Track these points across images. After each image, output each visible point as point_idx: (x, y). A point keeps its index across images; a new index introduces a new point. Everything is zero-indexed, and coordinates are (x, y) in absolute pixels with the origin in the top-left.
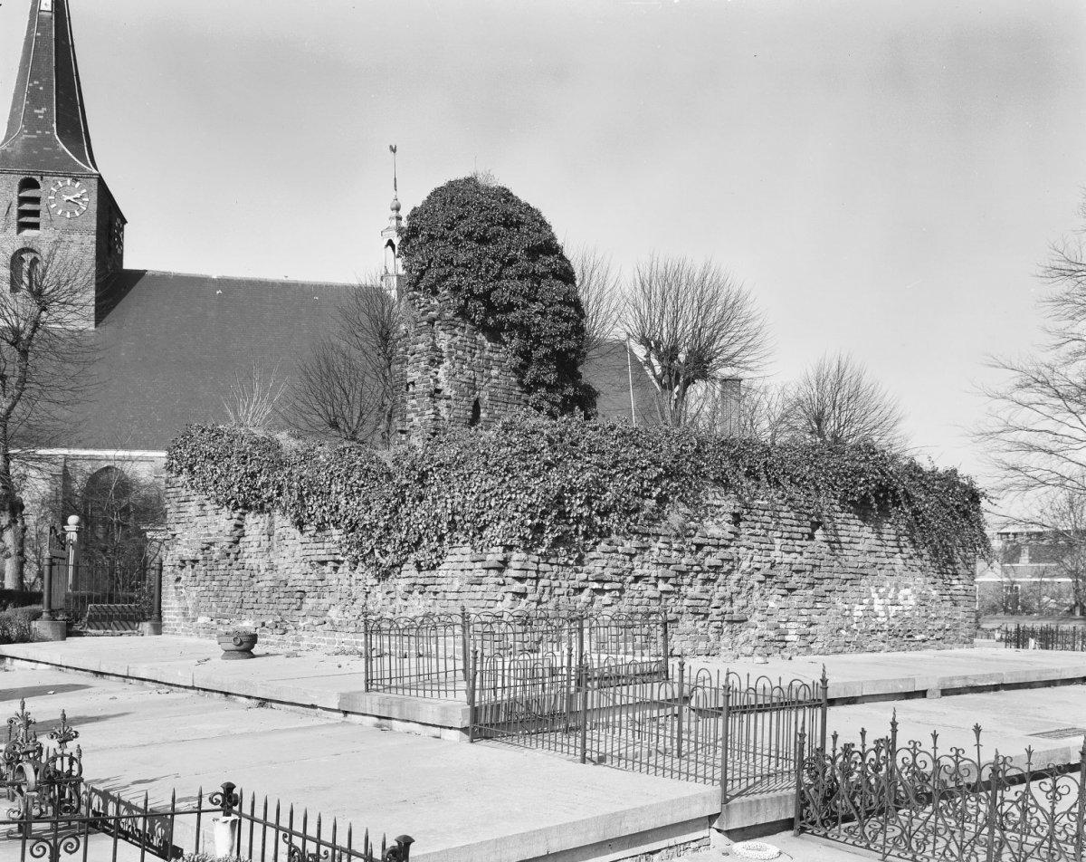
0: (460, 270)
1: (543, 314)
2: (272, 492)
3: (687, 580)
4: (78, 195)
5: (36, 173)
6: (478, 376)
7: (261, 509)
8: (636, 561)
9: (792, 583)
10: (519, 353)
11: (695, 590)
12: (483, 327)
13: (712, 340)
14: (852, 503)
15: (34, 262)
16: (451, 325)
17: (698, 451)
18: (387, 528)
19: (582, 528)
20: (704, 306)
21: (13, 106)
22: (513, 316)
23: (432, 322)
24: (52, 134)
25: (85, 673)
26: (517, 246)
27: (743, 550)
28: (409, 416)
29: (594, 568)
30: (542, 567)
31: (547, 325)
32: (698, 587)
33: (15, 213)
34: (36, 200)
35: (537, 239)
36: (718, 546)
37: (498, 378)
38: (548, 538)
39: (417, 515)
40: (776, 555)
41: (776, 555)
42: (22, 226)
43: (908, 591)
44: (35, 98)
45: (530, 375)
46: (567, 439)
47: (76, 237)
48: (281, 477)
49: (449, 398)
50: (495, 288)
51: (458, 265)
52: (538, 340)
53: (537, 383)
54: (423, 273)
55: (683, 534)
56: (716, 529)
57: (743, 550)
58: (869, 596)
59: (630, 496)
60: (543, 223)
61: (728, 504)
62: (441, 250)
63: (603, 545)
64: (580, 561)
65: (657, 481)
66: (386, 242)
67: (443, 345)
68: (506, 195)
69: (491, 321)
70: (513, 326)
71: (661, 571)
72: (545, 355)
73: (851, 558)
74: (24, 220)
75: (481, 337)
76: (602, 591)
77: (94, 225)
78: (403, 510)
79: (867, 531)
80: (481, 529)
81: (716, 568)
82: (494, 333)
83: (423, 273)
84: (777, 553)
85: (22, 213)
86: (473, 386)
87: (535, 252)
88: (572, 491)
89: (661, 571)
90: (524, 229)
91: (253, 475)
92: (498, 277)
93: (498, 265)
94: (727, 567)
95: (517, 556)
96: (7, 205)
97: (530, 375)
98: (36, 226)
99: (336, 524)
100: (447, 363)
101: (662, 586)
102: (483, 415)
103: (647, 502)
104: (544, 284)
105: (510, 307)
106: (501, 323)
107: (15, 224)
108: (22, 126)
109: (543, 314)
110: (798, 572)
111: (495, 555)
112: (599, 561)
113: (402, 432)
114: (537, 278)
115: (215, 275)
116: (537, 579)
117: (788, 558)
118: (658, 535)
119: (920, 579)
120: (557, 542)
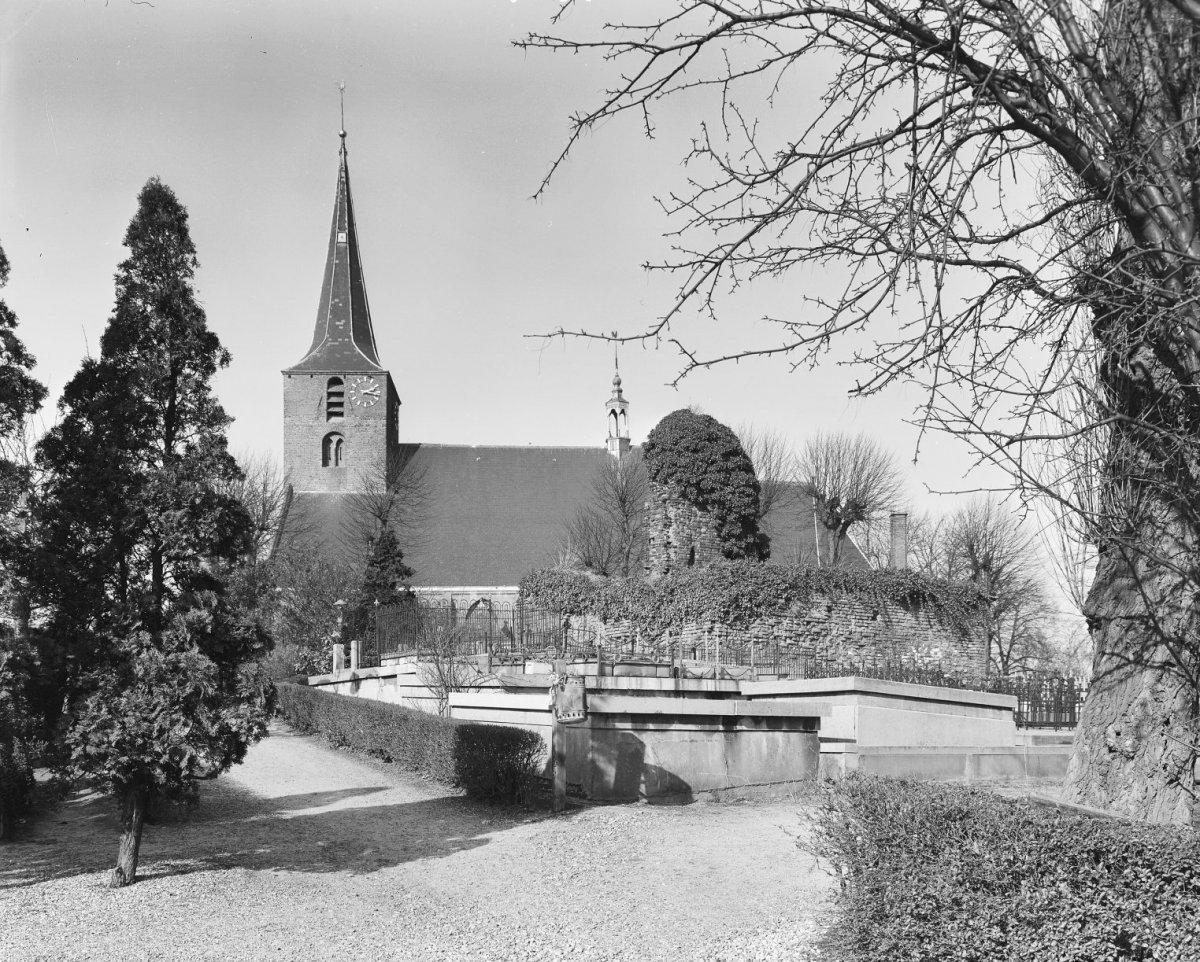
0: (682, 469)
1: (733, 493)
2: (588, 603)
3: (802, 639)
4: (372, 389)
5: (340, 373)
6: (694, 533)
7: (580, 613)
8: (775, 629)
9: (862, 642)
10: (718, 517)
11: (807, 644)
12: (696, 503)
13: (866, 489)
14: (897, 600)
15: (340, 442)
16: (676, 503)
17: (807, 575)
18: (654, 618)
19: (748, 612)
20: (858, 471)
21: (319, 319)
22: (715, 496)
23: (664, 501)
24: (350, 341)
25: (495, 690)
26: (717, 451)
27: (833, 625)
28: (651, 559)
29: (754, 632)
30: (729, 631)
31: (736, 501)
32: (808, 643)
33: (325, 405)
34: (340, 394)
35: (729, 448)
36: (818, 622)
37: (706, 533)
38: (732, 617)
39: (669, 610)
40: (852, 627)
41: (852, 627)
42: (330, 415)
43: (937, 650)
44: (337, 313)
45: (725, 531)
46: (740, 572)
47: (371, 422)
48: (593, 595)
49: (676, 547)
50: (703, 479)
51: (680, 467)
52: (730, 510)
53: (730, 536)
54: (658, 471)
55: (799, 616)
56: (818, 614)
57: (833, 625)
58: (911, 651)
59: (771, 598)
60: (733, 436)
61: (825, 602)
62: (669, 457)
63: (758, 621)
64: (747, 628)
65: (785, 590)
66: (609, 411)
67: (672, 515)
68: (709, 420)
69: (701, 499)
70: (714, 502)
71: (788, 634)
72: (735, 519)
73: (899, 631)
74: (332, 410)
75: (694, 509)
76: (757, 643)
77: (385, 412)
78: (662, 608)
79: (909, 616)
80: (701, 614)
81: (818, 634)
82: (702, 506)
83: (658, 471)
84: (853, 626)
85: (330, 405)
86: (690, 539)
87: (726, 456)
88: (743, 595)
89: (788, 634)
90: (720, 442)
91: (576, 595)
92: (705, 472)
93: (705, 465)
94: (824, 633)
95: (717, 625)
96: (319, 398)
97: (725, 531)
98: (341, 414)
99: (626, 617)
100: (674, 526)
101: (788, 641)
102: (697, 557)
103: (780, 600)
104: (733, 474)
105: (713, 490)
106: (707, 500)
107: (325, 414)
108: (327, 335)
109: (733, 493)
110: (865, 637)
111: (708, 625)
112: (757, 628)
113: (647, 568)
114: (728, 471)
115: (474, 443)
116: (727, 636)
117: (859, 630)
118: (786, 617)
119: (946, 644)
120: (736, 619)
